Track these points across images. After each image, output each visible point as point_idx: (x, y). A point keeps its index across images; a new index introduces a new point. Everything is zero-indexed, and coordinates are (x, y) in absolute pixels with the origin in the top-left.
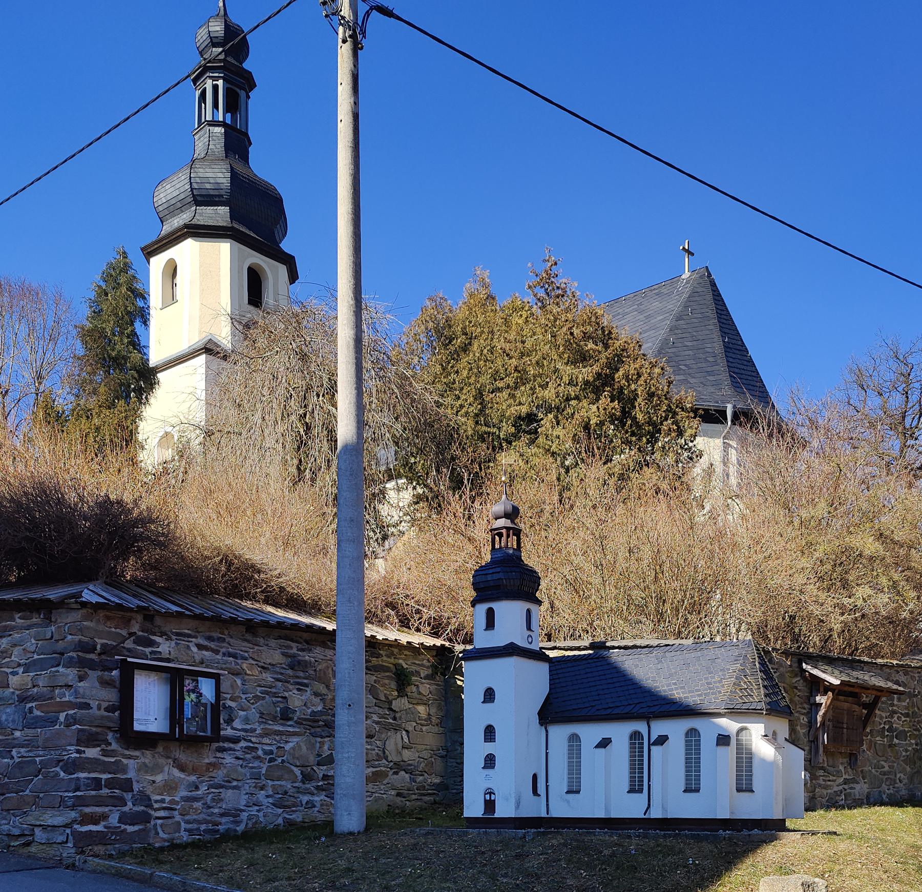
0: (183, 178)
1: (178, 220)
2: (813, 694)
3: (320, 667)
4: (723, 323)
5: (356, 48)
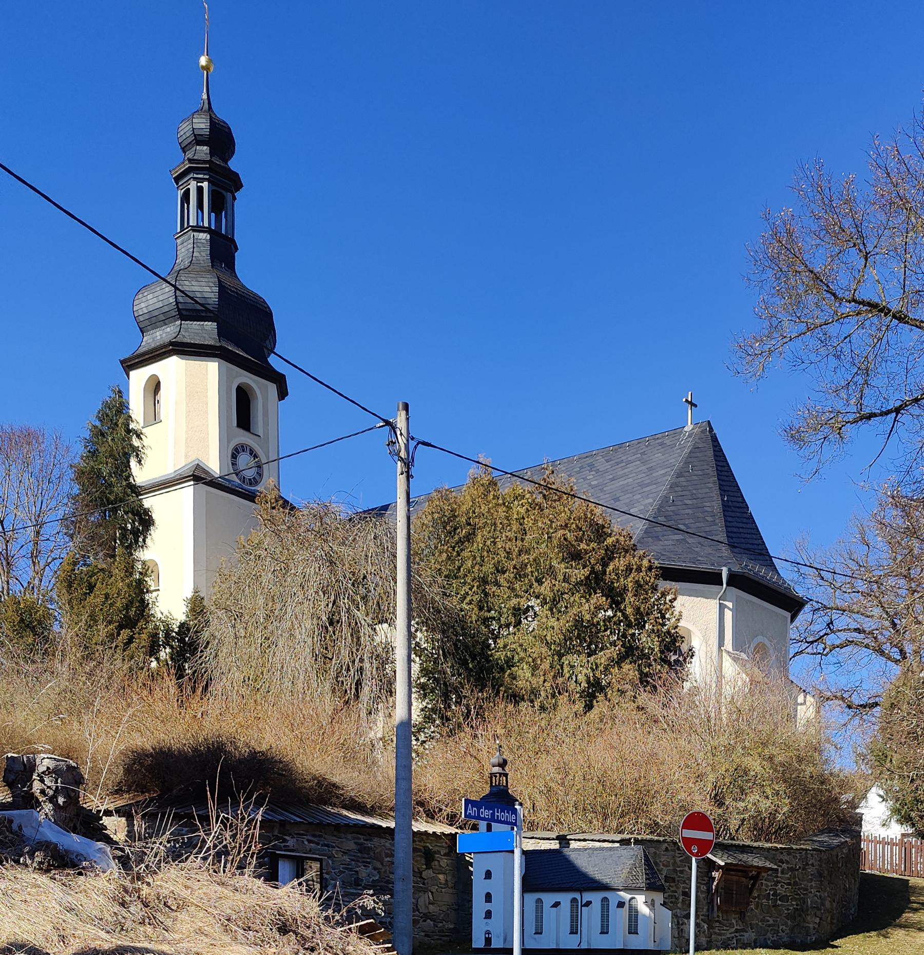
1: (161, 332)
3: (377, 851)
4: (723, 480)
5: (409, 477)
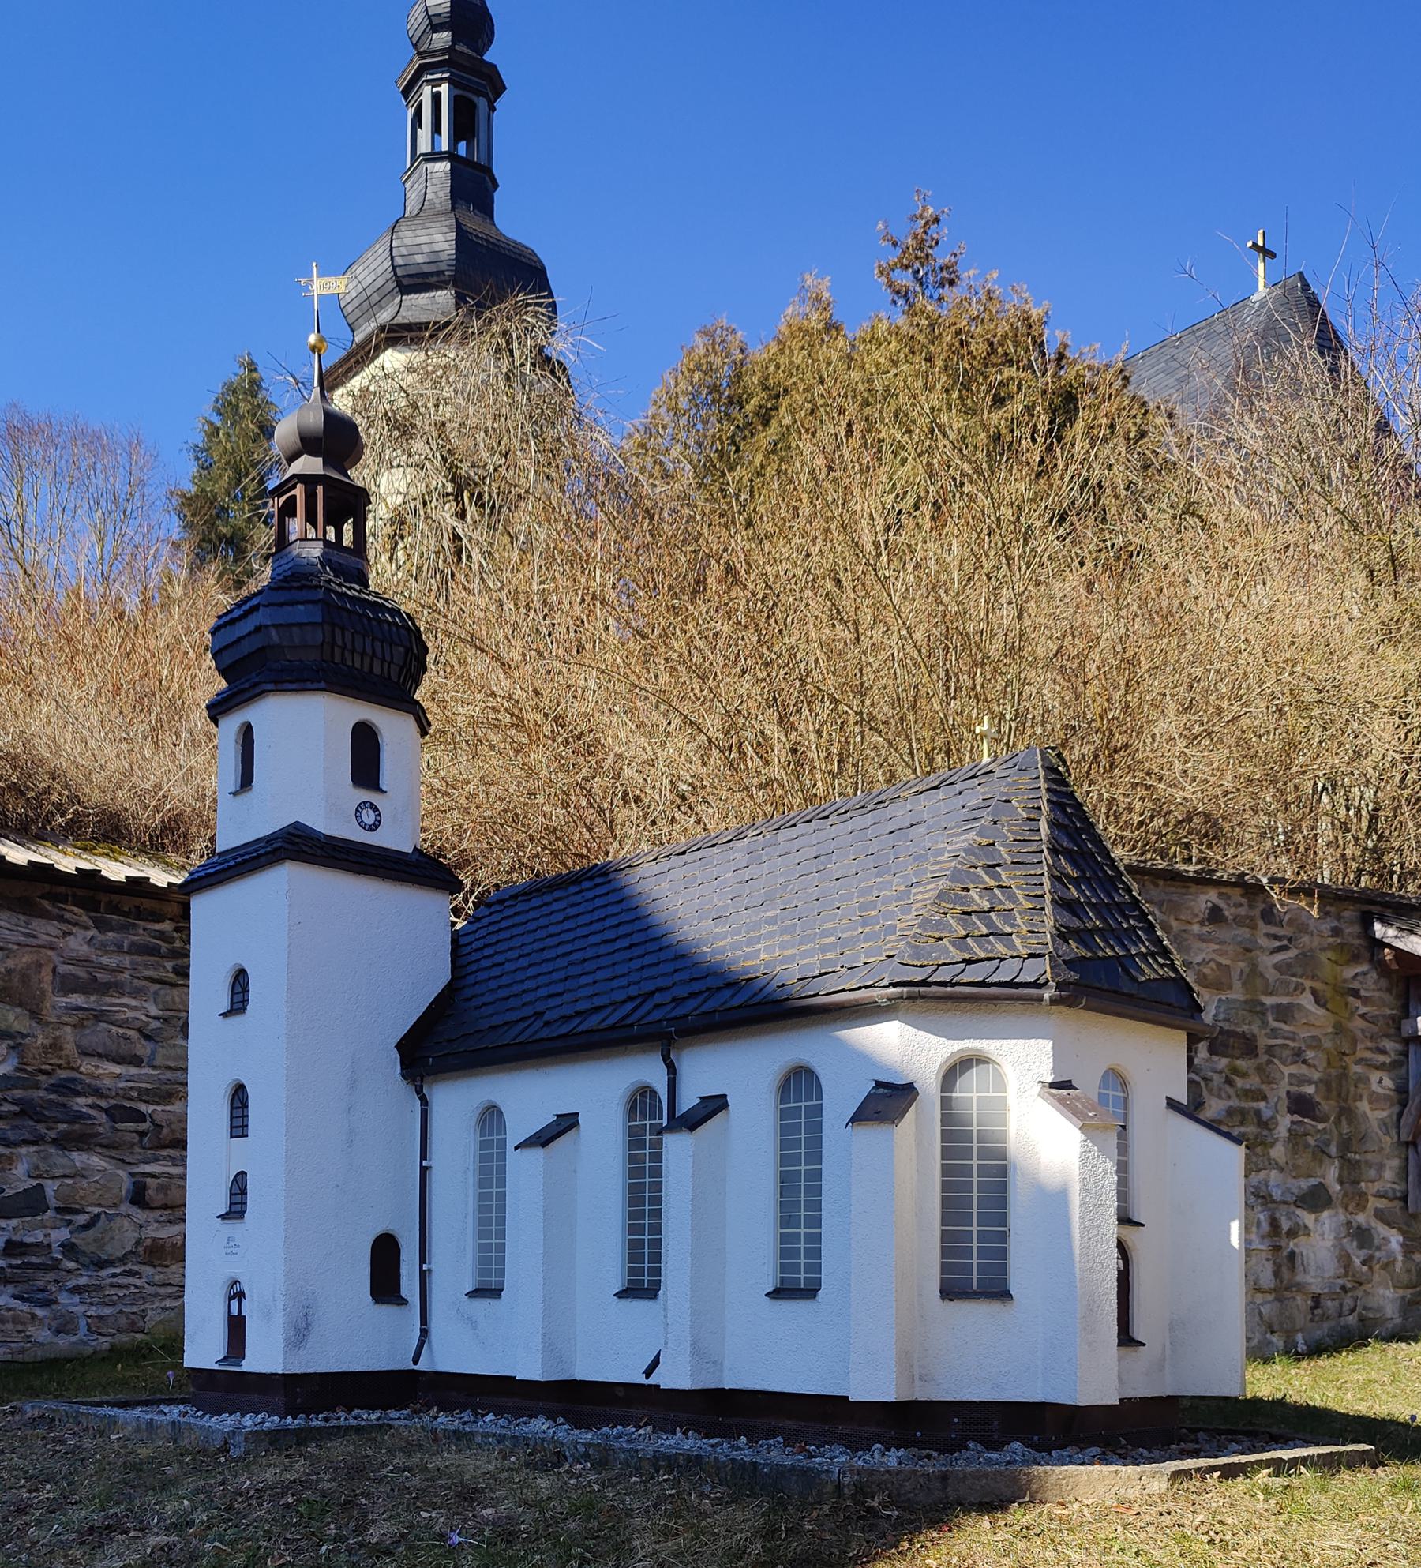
0: (381, 251)
2: (1413, 1012)
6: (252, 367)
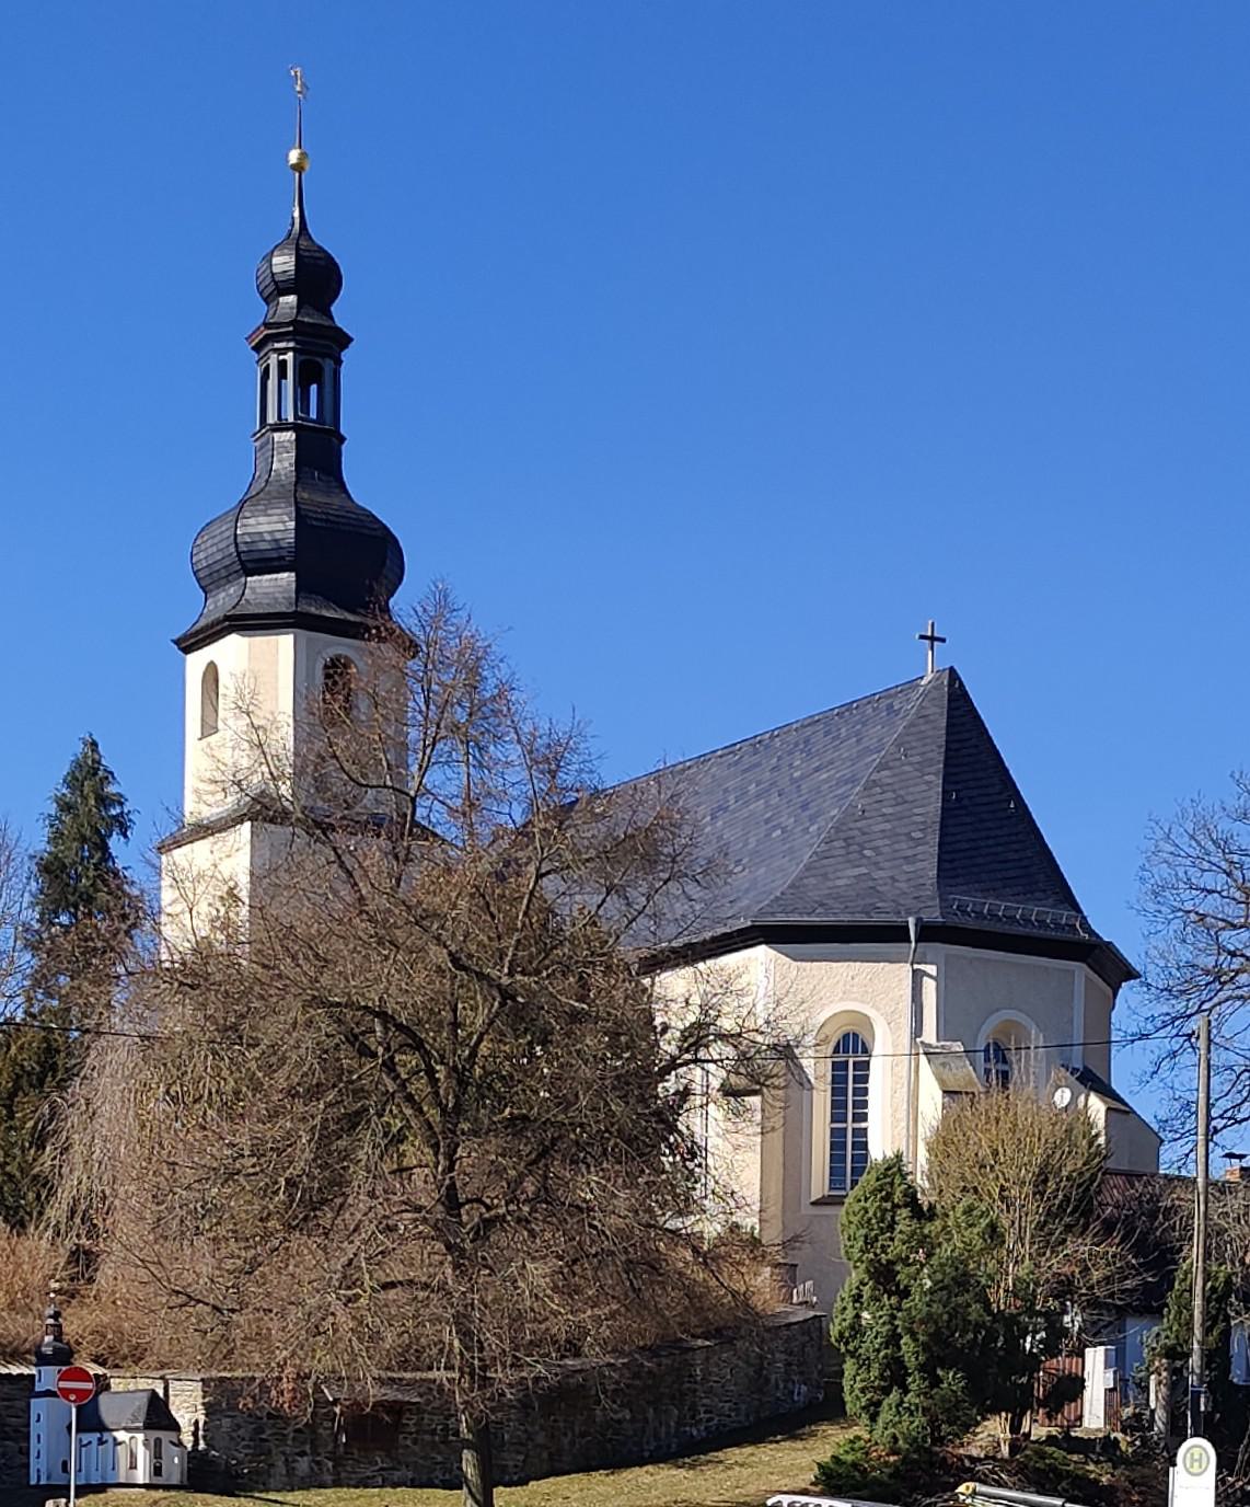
6: (94, 744)
